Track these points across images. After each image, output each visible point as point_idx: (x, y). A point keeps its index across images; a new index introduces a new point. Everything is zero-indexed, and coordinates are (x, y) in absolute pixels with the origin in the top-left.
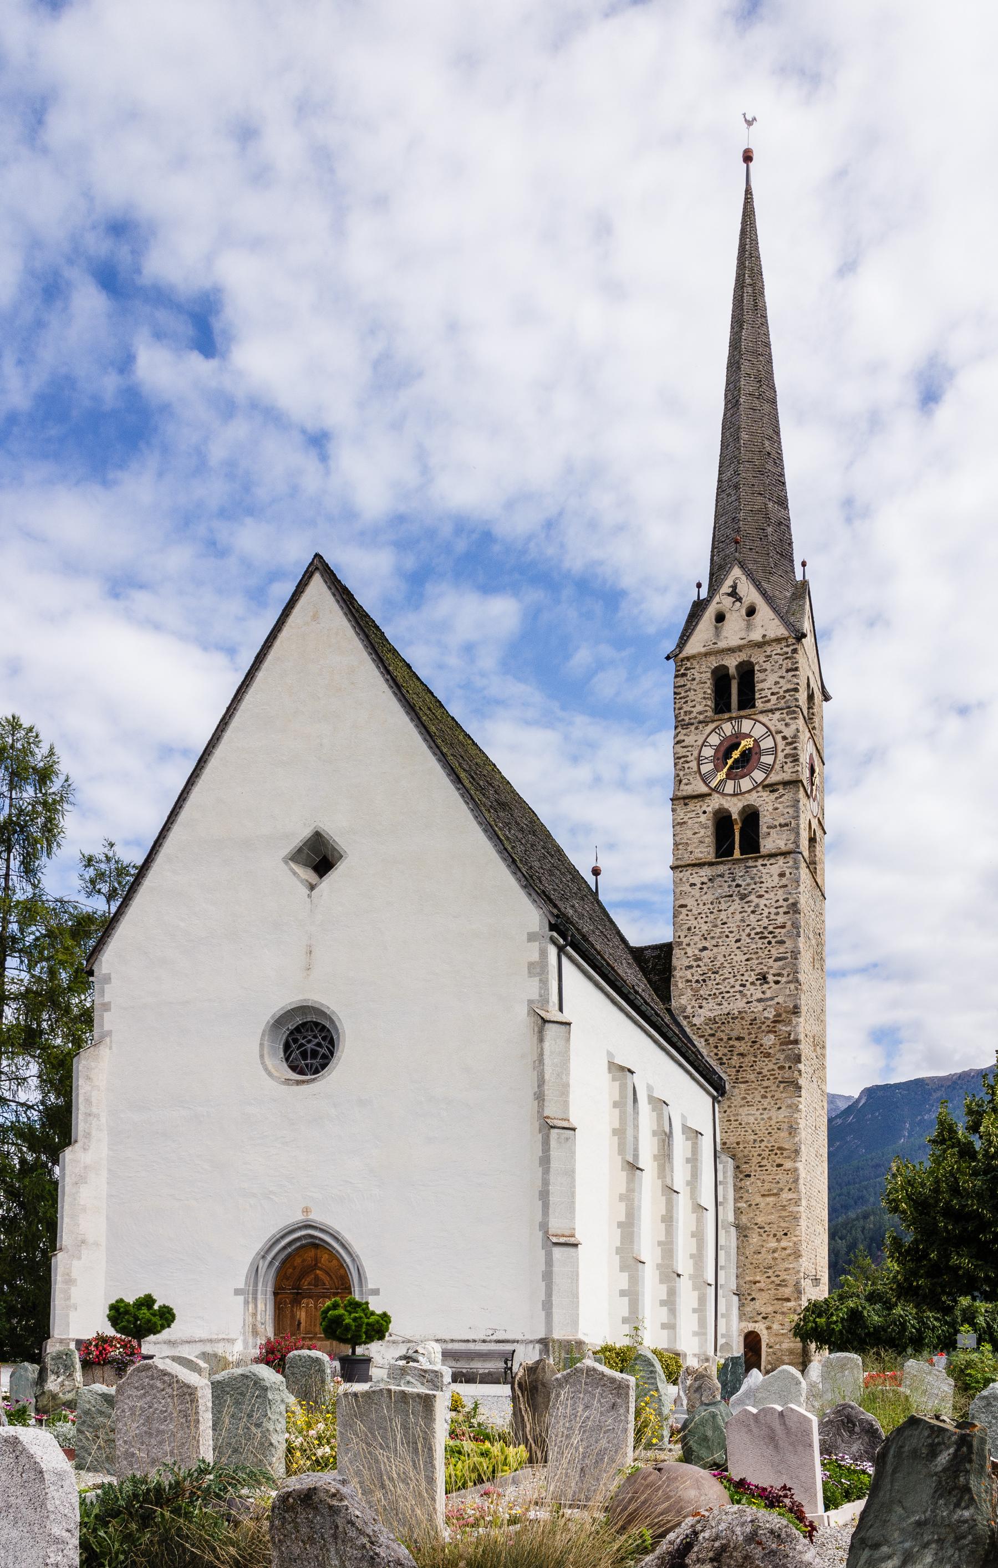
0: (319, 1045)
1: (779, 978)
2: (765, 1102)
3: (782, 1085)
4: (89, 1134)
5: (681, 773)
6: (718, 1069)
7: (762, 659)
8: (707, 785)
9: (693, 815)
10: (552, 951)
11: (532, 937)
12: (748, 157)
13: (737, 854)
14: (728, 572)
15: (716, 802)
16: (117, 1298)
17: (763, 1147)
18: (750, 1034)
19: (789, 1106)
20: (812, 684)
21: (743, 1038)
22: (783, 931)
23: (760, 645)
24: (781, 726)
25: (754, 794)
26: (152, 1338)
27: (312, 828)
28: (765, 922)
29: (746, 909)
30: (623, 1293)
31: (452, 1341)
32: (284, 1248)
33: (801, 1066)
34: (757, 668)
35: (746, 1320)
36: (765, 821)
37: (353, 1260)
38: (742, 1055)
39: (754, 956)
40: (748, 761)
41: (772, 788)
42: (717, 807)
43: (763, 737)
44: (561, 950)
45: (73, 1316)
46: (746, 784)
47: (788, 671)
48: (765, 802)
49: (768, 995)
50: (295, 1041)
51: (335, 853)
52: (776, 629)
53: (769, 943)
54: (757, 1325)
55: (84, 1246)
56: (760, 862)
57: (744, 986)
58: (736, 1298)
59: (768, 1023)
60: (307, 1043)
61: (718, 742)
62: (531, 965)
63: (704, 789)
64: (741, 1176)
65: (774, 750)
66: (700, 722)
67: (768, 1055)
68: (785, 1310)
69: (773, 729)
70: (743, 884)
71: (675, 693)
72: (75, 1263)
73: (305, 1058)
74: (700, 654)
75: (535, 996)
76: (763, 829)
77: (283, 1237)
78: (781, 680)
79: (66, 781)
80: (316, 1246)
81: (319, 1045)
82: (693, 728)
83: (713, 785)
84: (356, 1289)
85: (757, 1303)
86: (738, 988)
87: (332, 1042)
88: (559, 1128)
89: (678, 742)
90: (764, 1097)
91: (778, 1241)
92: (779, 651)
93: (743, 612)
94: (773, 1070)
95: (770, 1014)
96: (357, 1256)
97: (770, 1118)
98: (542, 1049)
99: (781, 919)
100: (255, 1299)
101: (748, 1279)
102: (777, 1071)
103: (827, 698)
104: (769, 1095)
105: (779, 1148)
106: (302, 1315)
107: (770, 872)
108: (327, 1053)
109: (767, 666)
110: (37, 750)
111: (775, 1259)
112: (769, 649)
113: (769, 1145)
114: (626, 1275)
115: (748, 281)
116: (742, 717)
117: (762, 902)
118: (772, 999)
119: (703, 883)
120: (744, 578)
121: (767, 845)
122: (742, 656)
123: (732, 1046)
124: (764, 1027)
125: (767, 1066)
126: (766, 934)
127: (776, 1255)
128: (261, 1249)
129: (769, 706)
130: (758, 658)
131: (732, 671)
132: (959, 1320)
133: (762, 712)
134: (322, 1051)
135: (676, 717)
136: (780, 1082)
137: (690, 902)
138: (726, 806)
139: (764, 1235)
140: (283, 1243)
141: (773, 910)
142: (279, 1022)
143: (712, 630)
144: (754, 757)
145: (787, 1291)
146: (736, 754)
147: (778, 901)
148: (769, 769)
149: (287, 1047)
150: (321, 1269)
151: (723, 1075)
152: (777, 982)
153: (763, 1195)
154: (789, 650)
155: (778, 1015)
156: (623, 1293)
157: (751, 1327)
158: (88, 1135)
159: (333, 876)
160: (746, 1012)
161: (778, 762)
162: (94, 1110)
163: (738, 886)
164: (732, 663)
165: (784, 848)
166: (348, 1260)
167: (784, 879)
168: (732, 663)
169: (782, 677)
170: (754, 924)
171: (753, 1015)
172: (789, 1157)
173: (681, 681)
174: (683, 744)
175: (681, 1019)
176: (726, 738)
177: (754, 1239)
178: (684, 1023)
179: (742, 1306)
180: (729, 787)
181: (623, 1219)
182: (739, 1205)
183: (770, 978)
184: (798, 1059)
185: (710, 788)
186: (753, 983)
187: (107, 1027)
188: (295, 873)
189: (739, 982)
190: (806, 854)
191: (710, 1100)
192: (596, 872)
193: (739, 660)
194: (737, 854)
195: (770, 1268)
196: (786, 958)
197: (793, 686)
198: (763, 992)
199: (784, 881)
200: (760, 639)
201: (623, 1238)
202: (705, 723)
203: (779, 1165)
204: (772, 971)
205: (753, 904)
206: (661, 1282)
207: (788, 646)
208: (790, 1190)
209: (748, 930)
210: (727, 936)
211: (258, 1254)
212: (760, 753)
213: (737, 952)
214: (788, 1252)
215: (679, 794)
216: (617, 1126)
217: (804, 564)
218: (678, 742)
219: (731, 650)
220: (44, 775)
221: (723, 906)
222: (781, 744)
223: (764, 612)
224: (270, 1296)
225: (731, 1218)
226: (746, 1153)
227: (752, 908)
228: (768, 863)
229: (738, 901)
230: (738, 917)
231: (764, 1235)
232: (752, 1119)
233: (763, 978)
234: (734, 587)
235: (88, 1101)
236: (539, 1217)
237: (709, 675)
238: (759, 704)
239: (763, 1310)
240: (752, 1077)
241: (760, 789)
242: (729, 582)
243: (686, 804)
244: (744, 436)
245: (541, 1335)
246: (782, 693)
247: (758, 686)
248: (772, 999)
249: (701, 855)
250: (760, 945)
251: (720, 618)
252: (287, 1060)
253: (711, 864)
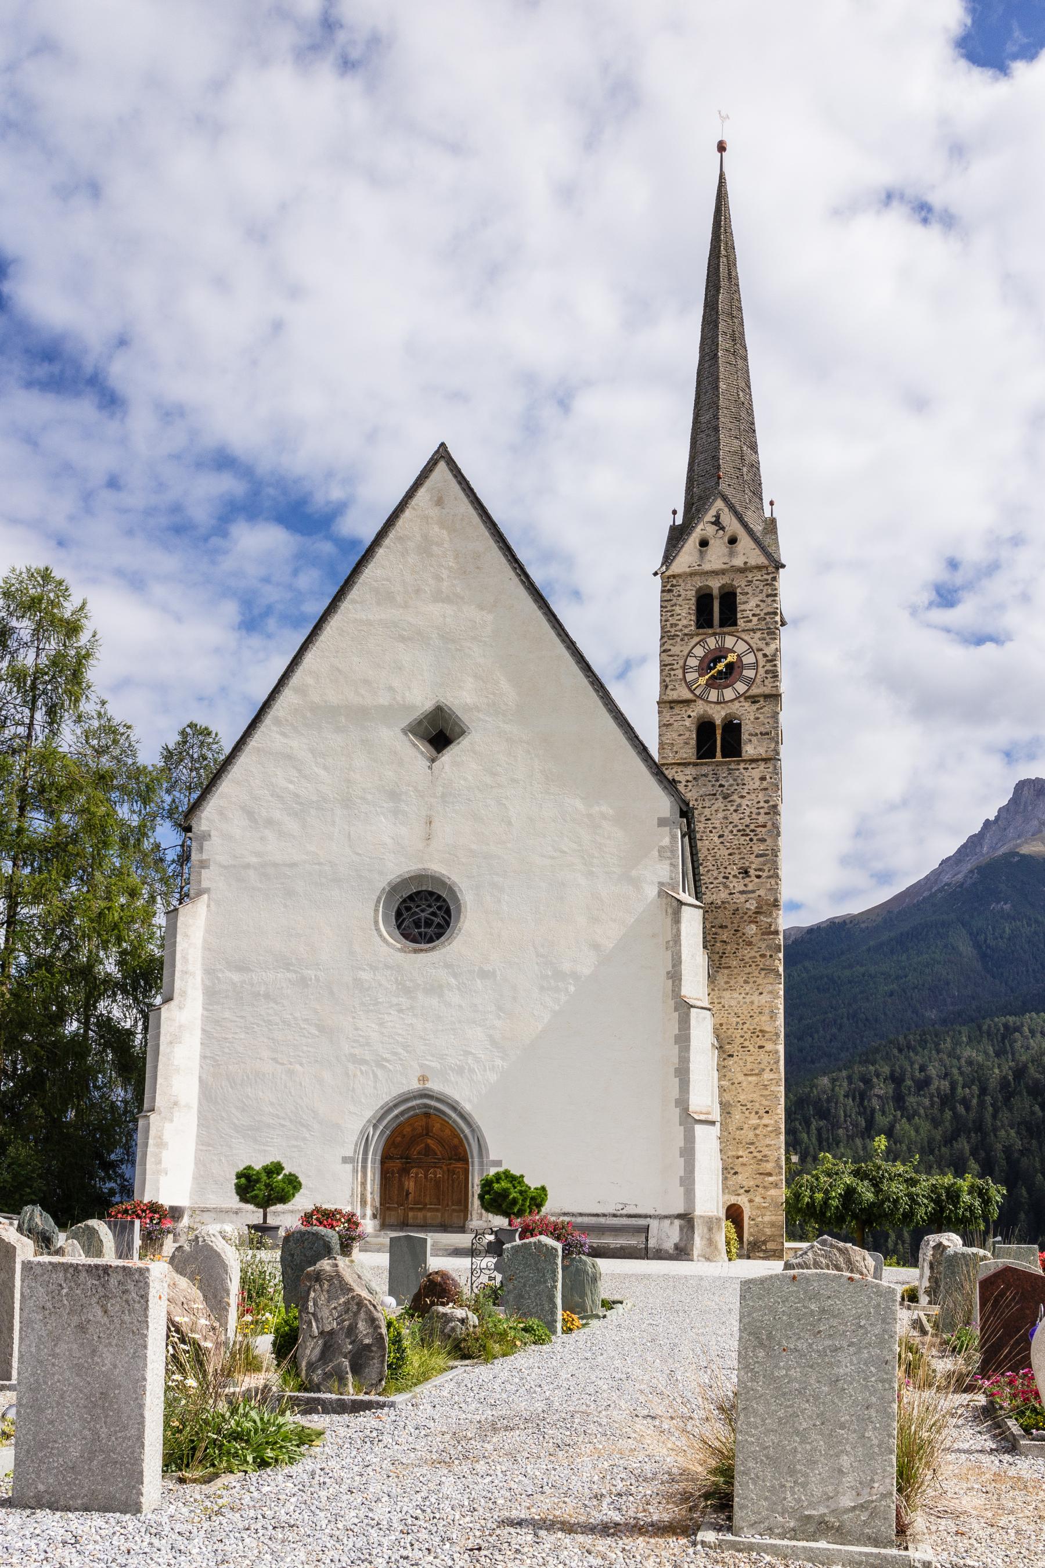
0: (433, 914)
1: (760, 873)
2: (747, 988)
3: (763, 973)
4: (184, 992)
5: (668, 679)
7: (743, 583)
8: (692, 692)
9: (679, 718)
11: (662, 822)
12: (721, 147)
13: (719, 758)
14: (712, 504)
15: (699, 709)
16: (248, 1164)
17: (745, 1029)
18: (732, 923)
19: (771, 992)
21: (726, 927)
22: (764, 830)
23: (744, 570)
25: (737, 704)
26: (279, 1207)
27: (434, 702)
28: (747, 821)
29: (729, 807)
31: (581, 1215)
32: (397, 1116)
34: (739, 590)
35: (729, 1193)
37: (473, 1131)
39: (736, 851)
40: (731, 673)
41: (754, 699)
42: (702, 712)
43: (746, 653)
45: (163, 1180)
46: (729, 694)
47: (768, 596)
48: (746, 713)
49: (750, 887)
51: (457, 729)
52: (756, 558)
53: (751, 840)
54: (739, 1198)
55: (176, 1109)
56: (742, 765)
57: (727, 878)
59: (750, 913)
60: (423, 913)
61: (702, 654)
63: (690, 696)
64: (725, 1056)
65: (755, 666)
66: (686, 635)
67: (750, 944)
68: (766, 1184)
69: (754, 646)
70: (726, 784)
71: (662, 607)
72: (167, 1125)
73: (418, 926)
74: (685, 573)
75: (666, 879)
76: (745, 737)
77: (396, 1106)
78: (761, 604)
79: (94, 636)
81: (433, 914)
82: (678, 639)
83: (697, 692)
84: (476, 1160)
85: (740, 1177)
86: (721, 879)
87: (448, 912)
88: (698, 1007)
89: (664, 651)
90: (746, 982)
91: (760, 1118)
92: (760, 578)
93: (726, 539)
94: (755, 957)
95: (752, 905)
96: (478, 1127)
97: (752, 1003)
98: (679, 930)
99: (762, 819)
100: (364, 1168)
101: (730, 1153)
102: (759, 959)
104: (751, 980)
105: (761, 1031)
106: (410, 1185)
107: (752, 775)
108: (442, 922)
109: (748, 589)
110: (65, 604)
111: (756, 1135)
112: (750, 576)
113: (752, 1028)
115: (723, 252)
116: (725, 634)
117: (745, 802)
118: (753, 892)
119: (687, 781)
120: (726, 510)
121: (749, 750)
122: (724, 580)
123: (716, 934)
124: (746, 917)
125: (747, 953)
126: (748, 832)
127: (757, 1132)
128: (373, 1117)
129: (750, 625)
130: (740, 582)
132: (944, 1198)
133: (743, 631)
134: (436, 920)
135: (662, 628)
136: (762, 969)
138: (710, 712)
139: (747, 1112)
140: (396, 1112)
141: (755, 811)
142: (394, 889)
143: (697, 554)
144: (736, 671)
146: (721, 666)
147: (759, 802)
148: (750, 682)
149: (399, 914)
150: (432, 1137)
152: (758, 877)
153: (745, 1075)
154: (769, 577)
157: (733, 1199)
158: (184, 993)
160: (728, 903)
161: (758, 676)
162: (191, 968)
163: (721, 786)
165: (764, 756)
166: (467, 1131)
167: (765, 783)
169: (764, 601)
170: (736, 821)
171: (736, 906)
172: (770, 1040)
173: (668, 596)
174: (669, 653)
176: (710, 651)
177: (737, 1116)
180: (713, 695)
182: (722, 1083)
183: (752, 872)
185: (695, 695)
186: (735, 876)
187: (205, 884)
188: (415, 745)
189: (722, 875)
193: (723, 582)
194: (719, 758)
195: (752, 1144)
196: (767, 855)
197: (772, 610)
198: (745, 885)
200: (742, 565)
202: (691, 636)
203: (761, 1047)
204: (754, 866)
205: (736, 804)
207: (768, 574)
208: (771, 1070)
209: (730, 827)
210: (711, 832)
211: (369, 1121)
212: (742, 667)
213: (721, 846)
214: (769, 1129)
215: (665, 698)
217: (772, 503)
218: (664, 651)
219: (715, 573)
220: (72, 629)
223: (745, 542)
224: (378, 1165)
226: (729, 1032)
227: (734, 808)
228: (750, 767)
229: (721, 800)
231: (747, 1112)
232: (733, 1003)
233: (746, 872)
234: (718, 517)
235: (185, 959)
236: (675, 1093)
237: (694, 592)
238: (740, 622)
239: (744, 1183)
241: (742, 699)
242: (712, 512)
243: (672, 708)
244: (722, 386)
245: (681, 1210)
246: (762, 615)
247: (740, 607)
248: (753, 892)
249: (685, 756)
250: (742, 841)
251: (704, 543)
252: (399, 927)
253: (695, 765)
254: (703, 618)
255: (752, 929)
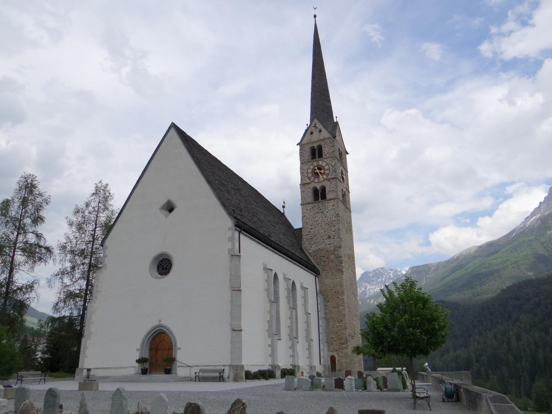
0: (167, 266)
6: (317, 266)
10: (237, 234)
11: (229, 229)
12: (315, 16)
15: (313, 185)
20: (341, 149)
23: (323, 140)
24: (330, 162)
28: (329, 220)
30: (269, 346)
32: (153, 334)
33: (343, 265)
36: (327, 190)
38: (324, 261)
41: (329, 180)
44: (240, 232)
48: (327, 184)
49: (331, 242)
50: (161, 264)
58: (326, 344)
62: (229, 238)
63: (309, 181)
65: (329, 169)
76: (327, 192)
77: (153, 330)
80: (164, 333)
87: (171, 265)
90: (332, 275)
95: (332, 248)
99: (334, 219)
103: (347, 153)
107: (330, 205)
112: (326, 141)
114: (270, 339)
117: (328, 214)
121: (328, 197)
122: (318, 143)
130: (323, 144)
131: (316, 148)
137: (306, 215)
145: (343, 341)
148: (328, 175)
149: (158, 267)
151: (319, 269)
155: (335, 249)
156: (269, 346)
157: (332, 354)
159: (174, 212)
164: (315, 145)
168: (315, 145)
175: (305, 251)
177: (332, 323)
178: (306, 252)
179: (329, 346)
181: (269, 319)
183: (332, 237)
184: (342, 262)
190: (341, 199)
191: (314, 277)
192: (284, 207)
199: (334, 207)
201: (269, 326)
206: (290, 340)
216: (266, 288)
221: (317, 216)
222: (331, 167)
225: (323, 315)
230: (321, 219)
234: (315, 125)
240: (328, 269)
247: (323, 151)
251: (312, 133)
253: (312, 203)
254: (313, 156)
255: (332, 256)
